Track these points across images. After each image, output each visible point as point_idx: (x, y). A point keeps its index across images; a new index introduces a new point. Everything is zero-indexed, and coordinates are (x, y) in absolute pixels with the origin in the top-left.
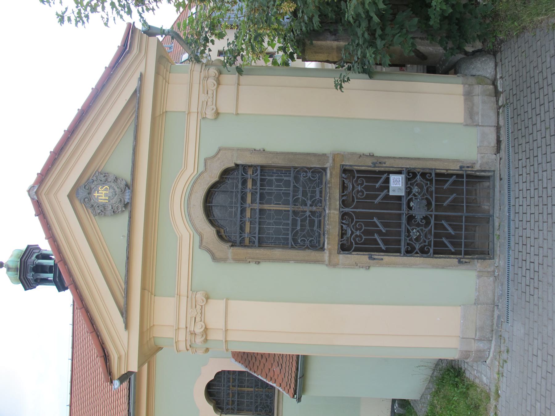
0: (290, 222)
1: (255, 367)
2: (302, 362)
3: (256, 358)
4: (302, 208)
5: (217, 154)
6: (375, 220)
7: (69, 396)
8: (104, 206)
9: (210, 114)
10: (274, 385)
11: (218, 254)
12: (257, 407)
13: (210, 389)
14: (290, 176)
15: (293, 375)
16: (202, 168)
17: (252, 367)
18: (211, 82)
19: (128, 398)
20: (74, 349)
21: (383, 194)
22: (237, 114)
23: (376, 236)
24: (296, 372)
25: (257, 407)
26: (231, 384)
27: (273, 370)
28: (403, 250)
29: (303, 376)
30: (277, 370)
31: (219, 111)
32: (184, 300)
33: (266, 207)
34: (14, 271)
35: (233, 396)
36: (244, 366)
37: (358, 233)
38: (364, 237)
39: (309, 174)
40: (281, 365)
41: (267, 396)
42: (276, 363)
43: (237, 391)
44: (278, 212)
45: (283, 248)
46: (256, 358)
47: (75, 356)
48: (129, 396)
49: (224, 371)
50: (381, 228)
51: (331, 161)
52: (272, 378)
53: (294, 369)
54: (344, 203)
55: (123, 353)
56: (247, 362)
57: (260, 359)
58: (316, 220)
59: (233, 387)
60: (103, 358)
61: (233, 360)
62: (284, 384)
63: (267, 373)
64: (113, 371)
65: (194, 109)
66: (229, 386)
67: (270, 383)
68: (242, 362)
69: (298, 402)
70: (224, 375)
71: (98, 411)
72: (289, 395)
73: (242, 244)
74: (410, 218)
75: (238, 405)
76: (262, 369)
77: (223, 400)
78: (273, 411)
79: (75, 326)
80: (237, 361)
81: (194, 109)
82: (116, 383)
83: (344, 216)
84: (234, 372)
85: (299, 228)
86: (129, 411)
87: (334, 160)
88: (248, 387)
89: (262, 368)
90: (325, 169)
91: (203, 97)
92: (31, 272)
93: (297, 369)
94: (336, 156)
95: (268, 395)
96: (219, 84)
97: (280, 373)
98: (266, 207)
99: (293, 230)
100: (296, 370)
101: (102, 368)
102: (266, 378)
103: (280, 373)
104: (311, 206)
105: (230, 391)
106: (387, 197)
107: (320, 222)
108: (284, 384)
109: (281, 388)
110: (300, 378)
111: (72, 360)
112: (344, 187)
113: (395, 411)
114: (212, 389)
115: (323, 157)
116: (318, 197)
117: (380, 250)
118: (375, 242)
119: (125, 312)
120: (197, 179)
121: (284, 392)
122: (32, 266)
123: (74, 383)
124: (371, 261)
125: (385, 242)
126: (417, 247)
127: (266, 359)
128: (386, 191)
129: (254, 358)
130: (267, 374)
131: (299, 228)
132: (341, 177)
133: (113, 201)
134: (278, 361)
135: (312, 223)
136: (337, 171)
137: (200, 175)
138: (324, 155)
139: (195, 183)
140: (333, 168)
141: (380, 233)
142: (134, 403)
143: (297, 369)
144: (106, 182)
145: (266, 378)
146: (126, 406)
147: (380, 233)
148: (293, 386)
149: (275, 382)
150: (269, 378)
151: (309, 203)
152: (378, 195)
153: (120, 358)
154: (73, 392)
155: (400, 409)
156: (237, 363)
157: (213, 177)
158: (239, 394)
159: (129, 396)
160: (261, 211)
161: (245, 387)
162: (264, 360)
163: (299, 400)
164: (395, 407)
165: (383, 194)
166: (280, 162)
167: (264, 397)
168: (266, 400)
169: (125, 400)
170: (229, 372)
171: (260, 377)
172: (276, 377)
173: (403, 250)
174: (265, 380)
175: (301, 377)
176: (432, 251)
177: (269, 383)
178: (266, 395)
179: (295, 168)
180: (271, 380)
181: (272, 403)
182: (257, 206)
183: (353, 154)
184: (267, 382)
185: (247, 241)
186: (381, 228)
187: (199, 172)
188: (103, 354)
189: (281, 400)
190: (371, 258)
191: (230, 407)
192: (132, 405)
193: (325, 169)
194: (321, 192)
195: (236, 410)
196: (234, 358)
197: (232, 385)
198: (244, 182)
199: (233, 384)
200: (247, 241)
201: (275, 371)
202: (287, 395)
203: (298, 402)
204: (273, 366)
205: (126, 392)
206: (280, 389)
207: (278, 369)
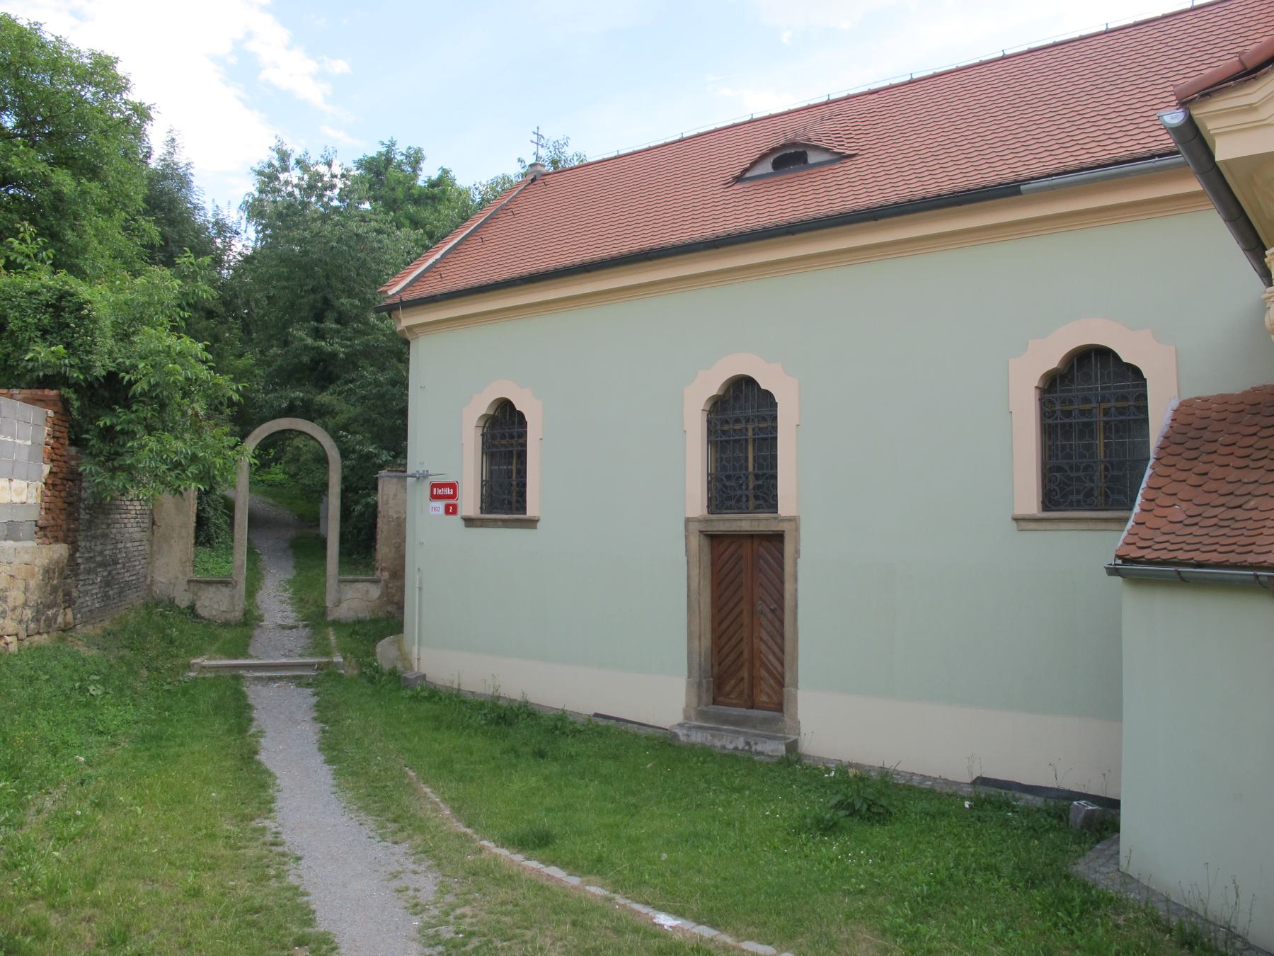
1: (1172, 460)
2: (1226, 577)
3: (1196, 459)
7: (1025, 48)
10: (1137, 509)
12: (1059, 469)
13: (1095, 355)
15: (1181, 556)
17: (1168, 450)
19: (1061, 170)
20: (1132, 29)
24: (1192, 561)
25: (1059, 469)
26: (1112, 404)
27: (1174, 505)
29: (1182, 582)
30: (1178, 512)
35: (1082, 413)
36: (1167, 432)
40: (1196, 524)
41: (1089, 494)
43: (1094, 419)
46: (1196, 459)
47: (1118, 35)
48: (1066, 172)
49: (1145, 386)
52: (1153, 503)
53: (1198, 557)
55: (1263, 114)
56: (1179, 439)
57: (1194, 470)
59: (1104, 409)
60: (1238, 68)
61: (1175, 404)
62: (1144, 532)
63: (1163, 489)
64: (1213, 100)
66: (1104, 400)
67: (1139, 499)
68: (1175, 425)
69: (1107, 568)
70: (1135, 386)
71: (1037, 109)
72: (1121, 546)
75: (1063, 425)
76: (1169, 476)
77: (1070, 391)
78: (1054, 508)
79: (1191, 14)
80: (1174, 415)
82: (1174, 117)
84: (1144, 409)
86: (1033, 179)
88: (1106, 445)
89: (1174, 477)
95: (1093, 495)
97: (1171, 522)
100: (1198, 562)
101: (1211, 75)
102: (1150, 488)
103: (1171, 522)
105: (1094, 405)
108: (1144, 532)
109: (1133, 526)
110: (1179, 572)
111: (1106, 32)
113: (1075, 803)
114: (1096, 359)
121: (1125, 534)
123: (1055, 51)
127: (1200, 486)
129: (1193, 454)
130: (1160, 488)
134: (1203, 515)
142: (1052, 187)
145: (1150, 488)
146: (1042, 170)
148: (1149, 554)
149: (1143, 510)
150: (1152, 494)
153: (1251, 108)
154: (1060, 47)
155: (1081, 816)
156: (1169, 413)
158: (1088, 425)
159: (1066, 172)
161: (1105, 438)
162: (1194, 479)
163: (1112, 571)
164: (1082, 802)
167: (1087, 485)
168: (1078, 492)
169: (1053, 166)
170: (1144, 397)
171: (1148, 472)
172: (1158, 511)
174: (1144, 485)
175: (1182, 574)
177: (1139, 495)
178: (1092, 489)
180: (1147, 500)
181: (1077, 506)
184: (1141, 491)
188: (1250, 65)
189: (1055, 526)
191: (1058, 407)
192: (1047, 183)
195: (1050, 421)
196: (1181, 404)
197: (1110, 408)
199: (1113, 410)
201: (1172, 508)
202: (1121, 542)
203: (1107, 568)
204: (1184, 505)
205: (1156, 147)
206: (1131, 523)
207: (1182, 517)
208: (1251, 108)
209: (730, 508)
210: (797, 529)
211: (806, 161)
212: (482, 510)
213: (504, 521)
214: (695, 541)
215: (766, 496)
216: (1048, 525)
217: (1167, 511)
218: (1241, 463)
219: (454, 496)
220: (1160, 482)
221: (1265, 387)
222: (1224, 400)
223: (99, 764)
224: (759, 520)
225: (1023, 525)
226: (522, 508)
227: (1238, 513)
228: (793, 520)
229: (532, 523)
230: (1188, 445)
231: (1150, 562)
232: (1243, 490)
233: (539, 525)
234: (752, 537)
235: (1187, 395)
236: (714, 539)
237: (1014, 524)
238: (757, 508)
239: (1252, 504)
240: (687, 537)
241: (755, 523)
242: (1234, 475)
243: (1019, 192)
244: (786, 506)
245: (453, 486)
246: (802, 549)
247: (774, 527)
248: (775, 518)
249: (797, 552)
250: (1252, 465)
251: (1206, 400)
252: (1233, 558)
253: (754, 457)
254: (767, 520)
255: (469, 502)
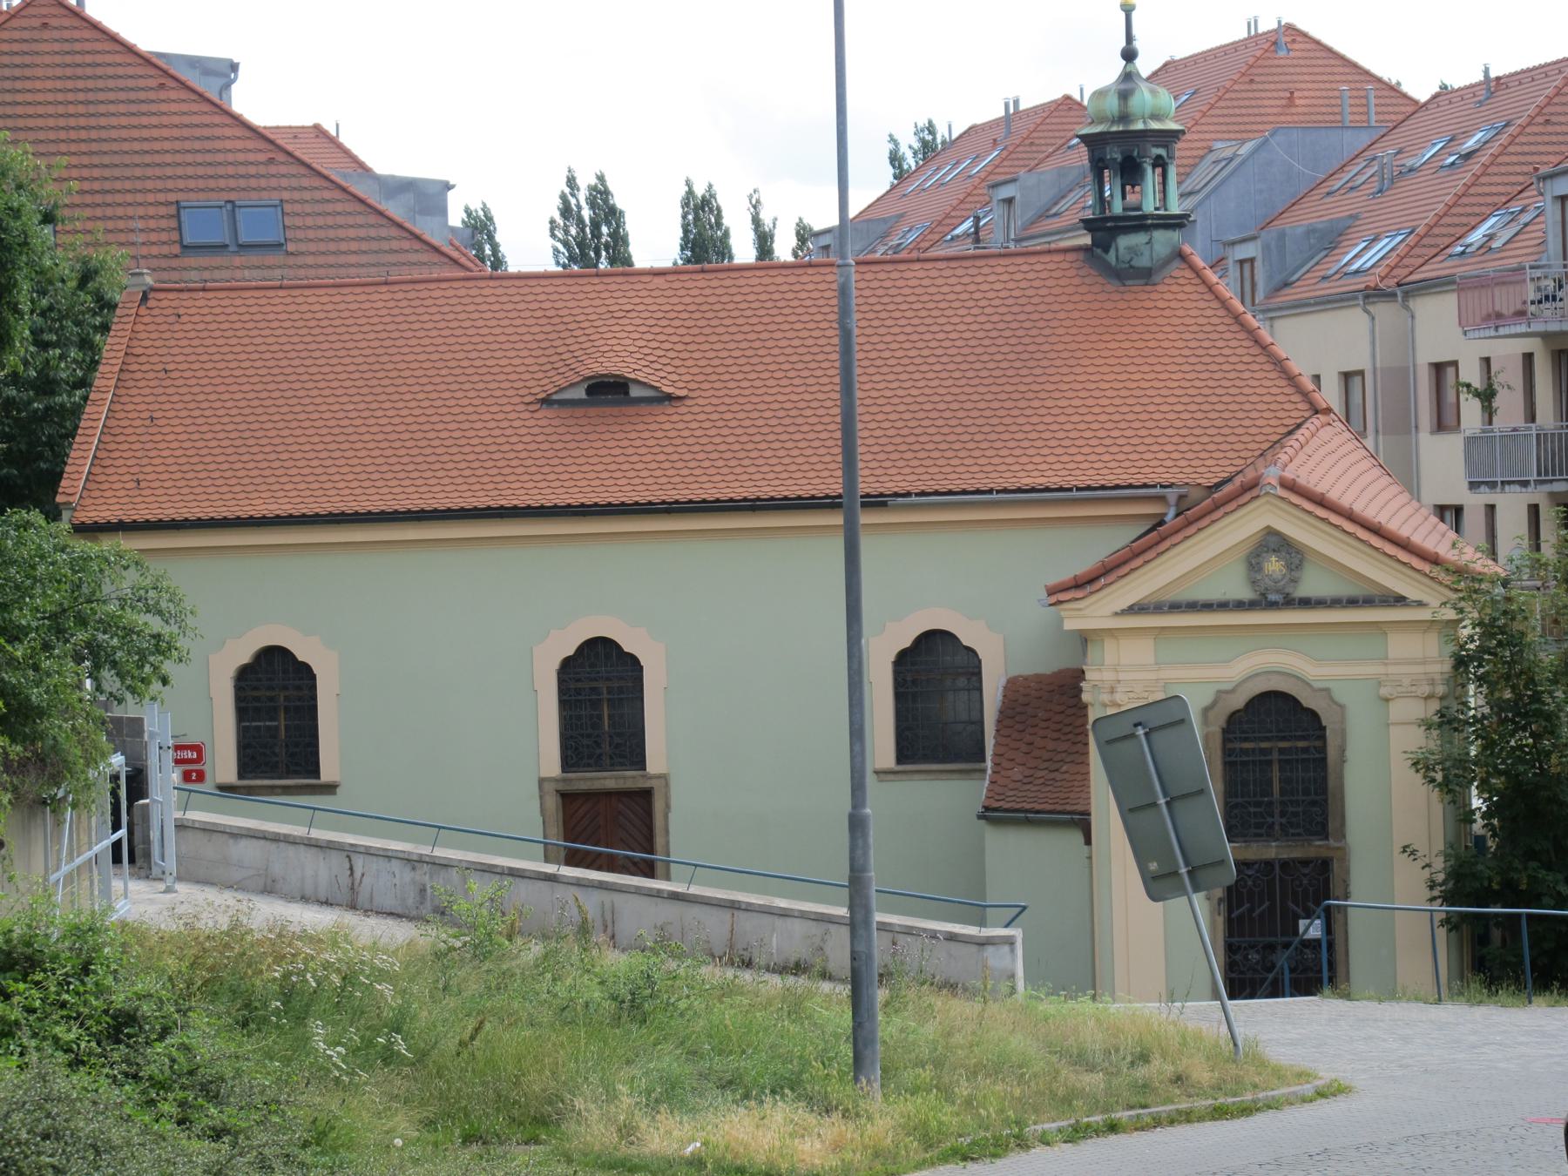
0: (1259, 799)
4: (1277, 811)
5: (1336, 703)
6: (1267, 904)
8: (1260, 570)
9: (1384, 691)
11: (1211, 714)
14: (1316, 794)
15: (1028, 806)
16: (1317, 685)
18: (1426, 690)
21: (1299, 911)
22: (1388, 725)
23: (1247, 906)
28: (1233, 940)
29: (1029, 822)
30: (1017, 773)
31: (1391, 704)
32: (1153, 676)
33: (1276, 767)
34: (1120, 111)
37: (1250, 883)
38: (1245, 891)
39: (1319, 819)
42: (1028, 772)
44: (1270, 783)
45: (1225, 792)
50: (1257, 912)
51: (1337, 845)
53: (1038, 807)
54: (1285, 865)
58: (1263, 831)
61: (1003, 681)
65: (1392, 669)
73: (1225, 741)
74: (1271, 948)
81: (1392, 669)
83: (1269, 864)
85: (1252, 810)
87: (1338, 848)
90: (1327, 838)
91: (1406, 682)
92: (1122, 153)
93: (1038, 812)
94: (1344, 853)
96: (1426, 698)
98: (1276, 767)
99: (1249, 803)
104: (1281, 824)
106: (1296, 918)
107: (1261, 835)
112: (1305, 862)
115: (1342, 835)
116: (1292, 831)
117: (1230, 911)
118: (1239, 905)
119: (1136, 609)
120: (1303, 681)
121: (987, 782)
122: (1135, 154)
124: (1216, 902)
125: (1241, 918)
126: (1238, 957)
128: (1303, 914)
131: (1252, 810)
132: (1317, 859)
133: (1267, 580)
135: (1258, 826)
136: (1325, 854)
137: (1308, 684)
138: (1344, 836)
139: (1298, 678)
140: (1328, 848)
141: (1251, 910)
143: (1038, 812)
144: (1289, 567)
147: (1251, 910)
151: (1270, 820)
152: (1297, 905)
153: (1080, 610)
157: (1307, 701)
160: (1270, 763)
162: (1024, 748)
163: (980, 817)
165: (1299, 911)
166: (1331, 783)
172: (1003, 773)
173: (1233, 940)
176: (1233, 975)
179: (1326, 801)
182: (1275, 756)
183: (1347, 872)
185: (1230, 746)
186: (1257, 912)
187: (1313, 683)
190: (1220, 900)
193: (1327, 838)
194: (1299, 834)
195: (902, 690)
196: (1008, 681)
198: (1303, 738)
200: (1230, 746)
204: (1021, 768)
207: (1021, 777)
208: (1080, 610)
209: (589, 765)
210: (667, 785)
211: (627, 393)
212: (241, 776)
213: (308, 786)
214: (553, 802)
215: (631, 750)
216: (904, 777)
217: (1009, 773)
218: (1055, 735)
219: (199, 760)
220: (1002, 750)
221: (1068, 670)
222: (1039, 678)
223: (379, 1008)
224: (625, 778)
225: (882, 776)
226: (315, 772)
227: (1056, 775)
228: (664, 778)
229: (330, 789)
230: (1017, 719)
231: (1007, 810)
232: (1059, 757)
233: (338, 790)
234: (609, 794)
235: (1014, 672)
236: (568, 799)
237: (875, 776)
238: (623, 766)
239: (1064, 768)
240: (541, 797)
241: (622, 781)
242: (1051, 745)
243: (884, 504)
244: (656, 761)
245: (197, 748)
246: (674, 802)
247: (647, 785)
248: (643, 776)
249: (668, 806)
250: (1063, 738)
251: (1026, 678)
252: (1059, 808)
253: (609, 716)
254: (634, 777)
255: (224, 763)
